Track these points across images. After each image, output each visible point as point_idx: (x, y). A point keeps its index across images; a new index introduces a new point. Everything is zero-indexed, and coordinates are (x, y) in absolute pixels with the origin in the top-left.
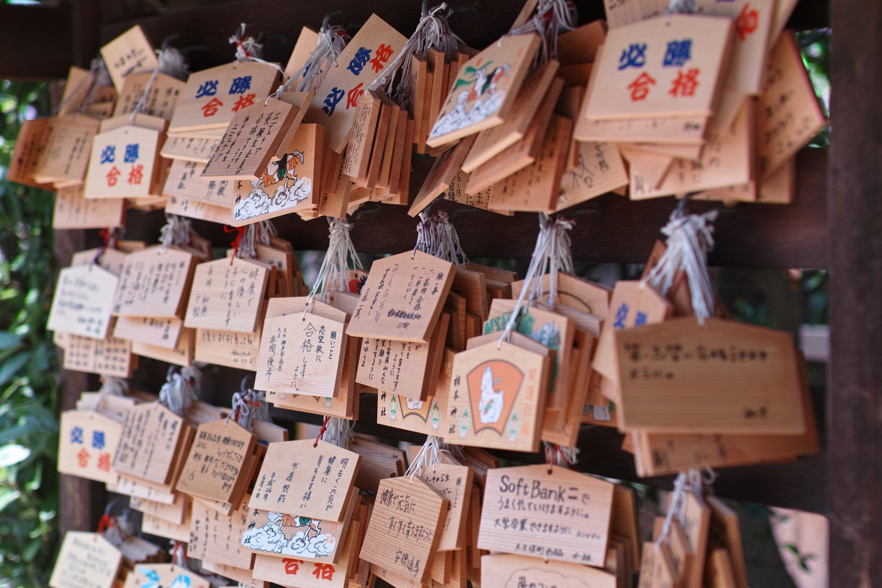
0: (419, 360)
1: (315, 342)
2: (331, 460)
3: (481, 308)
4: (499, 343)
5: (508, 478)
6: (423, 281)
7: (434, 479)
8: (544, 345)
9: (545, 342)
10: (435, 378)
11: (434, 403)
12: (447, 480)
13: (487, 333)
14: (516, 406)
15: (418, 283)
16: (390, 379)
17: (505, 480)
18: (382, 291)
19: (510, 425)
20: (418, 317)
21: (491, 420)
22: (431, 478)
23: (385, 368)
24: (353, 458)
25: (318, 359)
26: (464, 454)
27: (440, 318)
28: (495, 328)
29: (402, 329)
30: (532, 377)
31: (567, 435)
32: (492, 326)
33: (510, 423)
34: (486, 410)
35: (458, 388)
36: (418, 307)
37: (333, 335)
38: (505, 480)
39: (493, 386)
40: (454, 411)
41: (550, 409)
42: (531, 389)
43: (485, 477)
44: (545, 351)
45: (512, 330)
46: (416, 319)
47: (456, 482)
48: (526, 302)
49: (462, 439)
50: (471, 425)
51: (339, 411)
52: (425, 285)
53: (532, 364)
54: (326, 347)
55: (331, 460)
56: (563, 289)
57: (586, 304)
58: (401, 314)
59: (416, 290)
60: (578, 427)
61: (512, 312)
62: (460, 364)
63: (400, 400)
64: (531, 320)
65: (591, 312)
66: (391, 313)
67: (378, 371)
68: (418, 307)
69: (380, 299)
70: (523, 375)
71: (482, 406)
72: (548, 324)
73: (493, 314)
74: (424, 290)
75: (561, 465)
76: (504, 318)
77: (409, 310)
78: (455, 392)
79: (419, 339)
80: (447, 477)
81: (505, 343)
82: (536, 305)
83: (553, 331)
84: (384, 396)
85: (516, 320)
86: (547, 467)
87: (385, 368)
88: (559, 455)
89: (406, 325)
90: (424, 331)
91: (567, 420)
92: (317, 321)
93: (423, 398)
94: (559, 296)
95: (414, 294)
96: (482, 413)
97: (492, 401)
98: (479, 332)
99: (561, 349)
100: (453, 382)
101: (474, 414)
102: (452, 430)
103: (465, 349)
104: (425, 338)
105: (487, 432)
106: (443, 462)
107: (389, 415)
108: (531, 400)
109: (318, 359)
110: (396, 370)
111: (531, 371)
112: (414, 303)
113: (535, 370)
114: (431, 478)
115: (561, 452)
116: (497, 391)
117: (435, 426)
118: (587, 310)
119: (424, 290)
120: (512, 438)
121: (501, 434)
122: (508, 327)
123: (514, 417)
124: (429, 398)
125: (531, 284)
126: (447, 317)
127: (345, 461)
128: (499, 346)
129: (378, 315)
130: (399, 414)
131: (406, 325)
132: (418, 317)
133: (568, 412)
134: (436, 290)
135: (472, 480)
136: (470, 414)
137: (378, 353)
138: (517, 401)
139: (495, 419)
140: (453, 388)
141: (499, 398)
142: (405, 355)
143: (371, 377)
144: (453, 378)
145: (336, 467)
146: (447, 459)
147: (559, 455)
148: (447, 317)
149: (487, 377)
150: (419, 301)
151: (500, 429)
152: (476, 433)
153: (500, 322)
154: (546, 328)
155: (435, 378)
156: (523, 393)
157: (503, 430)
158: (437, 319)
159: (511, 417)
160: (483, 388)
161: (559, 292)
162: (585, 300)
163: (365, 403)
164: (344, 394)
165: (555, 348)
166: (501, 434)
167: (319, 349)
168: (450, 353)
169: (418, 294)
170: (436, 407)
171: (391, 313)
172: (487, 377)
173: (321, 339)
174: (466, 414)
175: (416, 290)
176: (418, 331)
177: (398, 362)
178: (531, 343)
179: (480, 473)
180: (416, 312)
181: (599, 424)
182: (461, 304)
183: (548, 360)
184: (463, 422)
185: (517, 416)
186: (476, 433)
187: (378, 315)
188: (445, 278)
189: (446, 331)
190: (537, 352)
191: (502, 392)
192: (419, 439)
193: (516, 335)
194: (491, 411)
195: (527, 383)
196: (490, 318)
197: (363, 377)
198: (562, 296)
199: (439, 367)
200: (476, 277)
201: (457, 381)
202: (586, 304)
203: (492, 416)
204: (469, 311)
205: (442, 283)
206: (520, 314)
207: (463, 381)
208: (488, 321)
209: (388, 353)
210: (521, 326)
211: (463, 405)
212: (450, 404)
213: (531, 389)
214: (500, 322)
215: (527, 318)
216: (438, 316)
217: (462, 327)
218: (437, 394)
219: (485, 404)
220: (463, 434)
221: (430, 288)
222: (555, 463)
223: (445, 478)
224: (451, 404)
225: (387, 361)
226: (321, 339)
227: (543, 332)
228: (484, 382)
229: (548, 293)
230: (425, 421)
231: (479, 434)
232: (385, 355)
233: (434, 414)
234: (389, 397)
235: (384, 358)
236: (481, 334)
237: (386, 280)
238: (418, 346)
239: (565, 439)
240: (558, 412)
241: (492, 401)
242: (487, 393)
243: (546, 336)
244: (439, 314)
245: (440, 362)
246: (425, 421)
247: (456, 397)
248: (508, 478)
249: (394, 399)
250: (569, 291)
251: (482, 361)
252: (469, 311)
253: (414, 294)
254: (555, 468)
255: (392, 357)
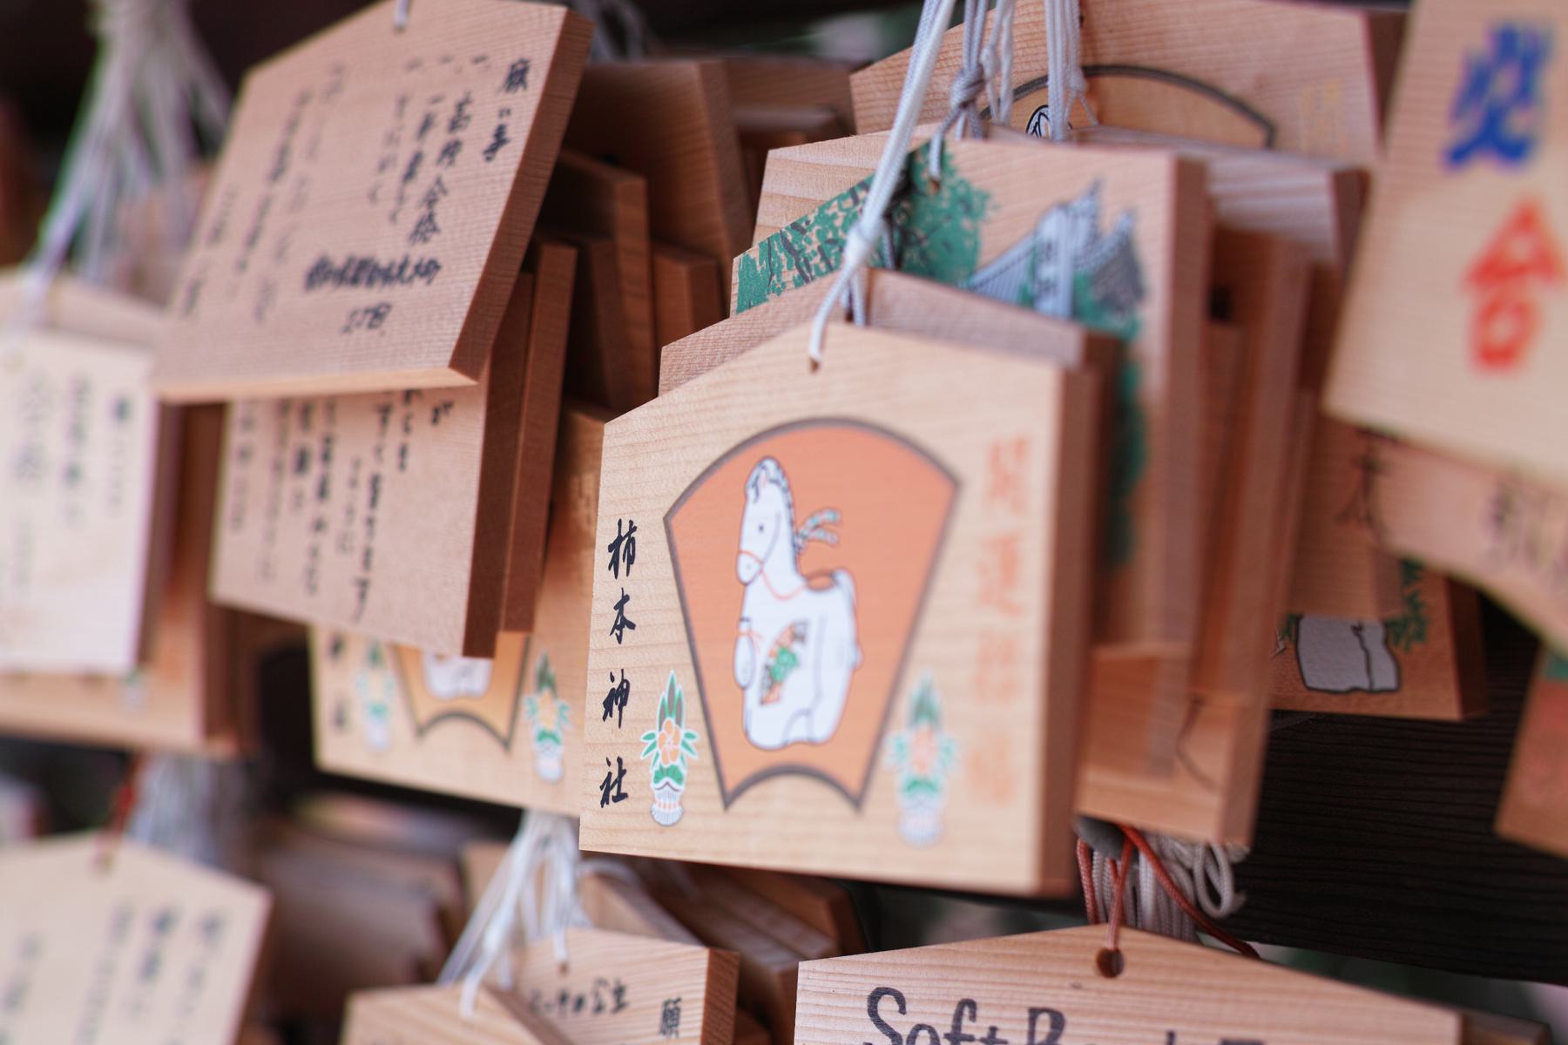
0: (443, 476)
1: (55, 447)
2: (163, 923)
3: (718, 218)
4: (809, 338)
5: (900, 999)
6: (445, 112)
7: (563, 998)
8: (1052, 317)
9: (1055, 303)
10: (525, 549)
11: (535, 665)
12: (620, 1006)
13: (746, 306)
14: (924, 648)
15: (426, 125)
16: (339, 570)
17: (887, 1007)
18: (284, 189)
19: (905, 749)
20: (428, 269)
21: (799, 731)
22: (550, 995)
23: (319, 526)
24: (242, 911)
25: (72, 515)
26: (682, 894)
27: (530, 264)
28: (790, 275)
29: (362, 334)
30: (1004, 485)
31: (1205, 781)
32: (772, 270)
33: (901, 735)
34: (772, 682)
35: (626, 583)
36: (426, 227)
37: (121, 410)
38: (887, 1007)
39: (798, 552)
40: (618, 697)
41: (1108, 654)
42: (1006, 550)
43: (791, 979)
44: (1068, 342)
45: (873, 268)
46: (419, 283)
47: (657, 1019)
48: (929, 132)
49: (663, 828)
50: (704, 757)
51: (167, 719)
52: (454, 125)
53: (998, 413)
54: (96, 464)
55: (163, 923)
56: (1110, 53)
57: (1240, 106)
58: (362, 271)
59: (417, 159)
60: (1257, 732)
61: (866, 186)
62: (637, 463)
63: (401, 660)
64: (968, 204)
65: (1271, 136)
66: (320, 273)
67: (293, 537)
68: (426, 227)
69: (275, 223)
70: (954, 482)
71: (749, 660)
72: (1064, 206)
73: (771, 217)
74: (451, 150)
75: (1160, 929)
76: (825, 220)
77: (388, 248)
78: (625, 610)
79: (431, 367)
80: (619, 992)
81: (839, 329)
82: (984, 124)
83: (1095, 237)
84: (337, 647)
85: (888, 216)
86: (1099, 937)
87: (319, 526)
88: (1146, 872)
89: (377, 315)
90: (453, 329)
91: (1196, 705)
92: (58, 360)
93: (478, 642)
94: (1092, 92)
95: (410, 175)
96: (753, 696)
97: (797, 634)
98: (712, 305)
99: (1152, 323)
100: (602, 556)
101: (710, 702)
102: (612, 791)
103: (655, 395)
104: (461, 359)
105: (783, 787)
106: (604, 923)
107: (364, 725)
108: (1011, 609)
109: (72, 515)
110: (358, 527)
111: (995, 454)
112: (412, 215)
113: (1021, 447)
114: (550, 995)
115: (1159, 860)
116: (818, 579)
117: (549, 765)
118: (1255, 135)
119: (451, 150)
120: (920, 820)
121: (857, 801)
122: (855, 249)
123: (924, 711)
124: (508, 642)
125: (940, 57)
126: (560, 262)
127: (211, 927)
128: (813, 351)
129: (267, 291)
130: (400, 726)
131: (377, 315)
132: (428, 269)
133: (1201, 666)
134: (500, 138)
135: (730, 997)
136: (692, 708)
137: (289, 458)
138: (932, 622)
139: (822, 727)
140: (603, 585)
141: (831, 614)
142: (391, 454)
143: (266, 571)
144: (604, 534)
145: (180, 952)
146: (619, 907)
147: (1146, 872)
148: (560, 262)
149: (767, 510)
150: (431, 201)
151: (852, 780)
152: (729, 798)
153: (811, 244)
154: (1052, 228)
155: (525, 549)
156: (959, 579)
157: (867, 780)
158: (514, 269)
159: (904, 707)
160: (746, 568)
161: (1091, 71)
162: (1233, 88)
163: (266, 679)
164: (184, 648)
165: (1114, 323)
166: (857, 801)
167: (73, 474)
168: (583, 420)
169: (428, 173)
170: (545, 680)
171: (320, 273)
172: (767, 510)
173: (77, 432)
174: (673, 707)
175: (417, 159)
176: (422, 341)
177: (363, 493)
178: (981, 312)
179: (769, 961)
180: (420, 252)
181: (1334, 706)
182: (627, 201)
183: (1089, 383)
184: (659, 745)
185: (937, 700)
186: (729, 798)
187: (267, 291)
188: (537, 80)
189: (561, 325)
190: (1015, 346)
191: (843, 578)
192: (501, 822)
193: (898, 288)
194: (796, 686)
195: (976, 521)
196: (760, 237)
197: (255, 566)
198: (1109, 83)
199: (544, 496)
200: (686, 73)
201: (624, 550)
202: (1240, 106)
203: (803, 709)
204: (665, 232)
205: (526, 103)
206: (907, 187)
207: (651, 545)
208: (754, 253)
209: (326, 457)
210: (918, 232)
211: (655, 660)
212: (594, 661)
213: (1006, 550)
214: (811, 244)
215: (945, 201)
216: (519, 255)
217: (637, 309)
218: (543, 620)
219: (764, 648)
220: (666, 807)
221: (477, 135)
222: (1130, 916)
223: (609, 1000)
224: (604, 656)
225: (323, 492)
226: (77, 432)
227: (1041, 253)
228: (751, 540)
229: (1040, 82)
230: (506, 743)
231: (739, 806)
232: (315, 469)
233: (540, 710)
234: (355, 653)
235: (309, 483)
236: (724, 314)
237: (300, 143)
238: (442, 406)
239: (1195, 807)
240: (1150, 663)
241: (797, 634)
242: (774, 596)
243: (1056, 271)
244: (523, 243)
245: (546, 472)
246: (506, 743)
247: (622, 624)
248: (900, 999)
249: (374, 658)
250: (1144, 57)
251: (736, 438)
252: (665, 232)
253: (410, 175)
254: (1131, 941)
255: (340, 471)
